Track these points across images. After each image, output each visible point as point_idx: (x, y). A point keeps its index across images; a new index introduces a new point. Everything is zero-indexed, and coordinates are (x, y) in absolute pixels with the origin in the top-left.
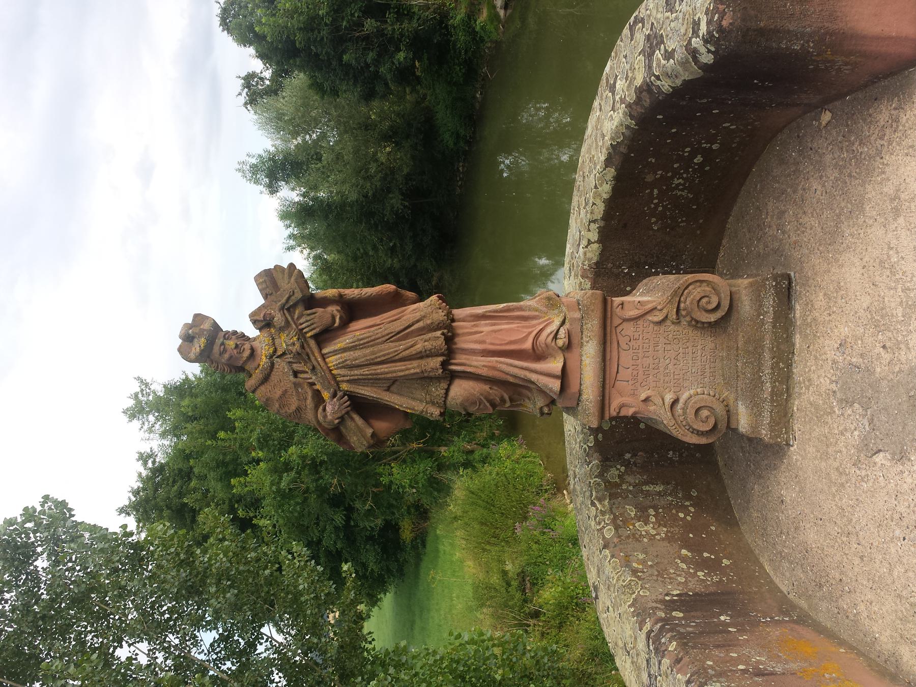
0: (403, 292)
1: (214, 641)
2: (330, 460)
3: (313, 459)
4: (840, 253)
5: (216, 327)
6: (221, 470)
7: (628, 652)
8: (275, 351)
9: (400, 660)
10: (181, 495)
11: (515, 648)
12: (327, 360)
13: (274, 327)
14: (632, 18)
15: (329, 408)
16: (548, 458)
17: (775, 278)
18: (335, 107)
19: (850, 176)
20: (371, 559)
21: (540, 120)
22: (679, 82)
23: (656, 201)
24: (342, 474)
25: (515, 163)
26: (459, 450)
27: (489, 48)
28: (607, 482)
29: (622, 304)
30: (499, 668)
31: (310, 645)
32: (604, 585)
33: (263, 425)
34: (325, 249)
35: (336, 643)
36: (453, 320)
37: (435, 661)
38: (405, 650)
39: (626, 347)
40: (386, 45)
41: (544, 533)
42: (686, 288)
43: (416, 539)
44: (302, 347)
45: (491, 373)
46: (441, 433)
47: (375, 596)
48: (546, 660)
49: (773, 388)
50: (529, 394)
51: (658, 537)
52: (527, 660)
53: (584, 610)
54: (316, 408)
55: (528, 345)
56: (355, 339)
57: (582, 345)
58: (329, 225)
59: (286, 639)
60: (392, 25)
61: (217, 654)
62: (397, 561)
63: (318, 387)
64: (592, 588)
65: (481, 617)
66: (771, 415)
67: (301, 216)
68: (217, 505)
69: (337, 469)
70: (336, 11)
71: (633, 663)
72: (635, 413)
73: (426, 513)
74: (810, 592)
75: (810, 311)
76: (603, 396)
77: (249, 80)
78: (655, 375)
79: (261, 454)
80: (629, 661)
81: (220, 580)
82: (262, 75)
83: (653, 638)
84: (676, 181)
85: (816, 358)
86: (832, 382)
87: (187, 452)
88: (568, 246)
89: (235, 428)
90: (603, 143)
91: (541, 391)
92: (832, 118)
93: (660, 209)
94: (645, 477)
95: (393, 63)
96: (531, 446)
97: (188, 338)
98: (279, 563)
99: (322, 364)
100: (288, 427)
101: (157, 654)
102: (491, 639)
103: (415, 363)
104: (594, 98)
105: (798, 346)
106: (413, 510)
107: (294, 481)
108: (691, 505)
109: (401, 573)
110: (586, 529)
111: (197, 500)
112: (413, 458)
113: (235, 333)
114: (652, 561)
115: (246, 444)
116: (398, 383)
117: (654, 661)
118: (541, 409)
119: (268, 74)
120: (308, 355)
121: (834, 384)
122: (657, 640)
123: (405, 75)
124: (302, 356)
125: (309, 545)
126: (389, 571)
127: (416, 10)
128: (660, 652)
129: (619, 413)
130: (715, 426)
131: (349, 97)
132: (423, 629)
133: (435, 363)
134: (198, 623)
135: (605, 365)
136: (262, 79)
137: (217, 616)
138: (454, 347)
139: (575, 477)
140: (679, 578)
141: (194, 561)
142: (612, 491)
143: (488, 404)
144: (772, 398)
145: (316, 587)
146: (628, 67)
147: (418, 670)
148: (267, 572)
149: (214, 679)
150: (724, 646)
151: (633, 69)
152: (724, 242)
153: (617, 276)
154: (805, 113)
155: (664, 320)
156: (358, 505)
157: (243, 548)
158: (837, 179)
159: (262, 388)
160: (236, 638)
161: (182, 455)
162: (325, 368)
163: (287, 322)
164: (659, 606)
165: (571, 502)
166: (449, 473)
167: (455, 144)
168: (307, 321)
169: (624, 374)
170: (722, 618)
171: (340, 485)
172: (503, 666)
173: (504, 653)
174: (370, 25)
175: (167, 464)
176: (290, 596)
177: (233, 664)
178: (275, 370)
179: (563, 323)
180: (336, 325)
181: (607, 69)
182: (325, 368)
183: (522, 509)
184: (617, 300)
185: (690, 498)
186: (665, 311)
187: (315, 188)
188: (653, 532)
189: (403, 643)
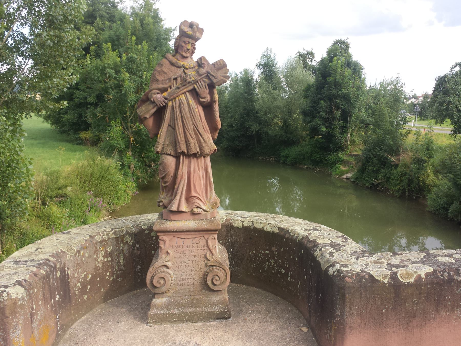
0: (218, 132)
1: (24, 35)
2: (123, 94)
3: (122, 86)
4: (242, 341)
5: (197, 40)
6: (115, 37)
7: (37, 250)
8: (187, 69)
9: (17, 133)
10: (101, 16)
11: (26, 193)
12: (183, 95)
13: (198, 69)
14: (347, 237)
15: (159, 96)
16: (128, 207)
17: (229, 311)
18: (299, 97)
19: (278, 342)
20: (69, 117)
21: (296, 197)
22: (319, 259)
23: (263, 252)
24: (115, 101)
25: (275, 185)
26: (130, 161)
27: (328, 171)
28: (124, 236)
29: (215, 239)
30: (14, 185)
31: (24, 85)
32: (71, 237)
33: (140, 60)
34: (230, 92)
35: (25, 98)
36: (204, 157)
37: (17, 152)
38: (22, 135)
39: (194, 242)
40: (328, 121)
41: (88, 206)
42: (223, 269)
43: (81, 140)
44: (189, 83)
45: (179, 176)
46: (139, 152)
47: (49, 119)
48: (20, 209)
49: (175, 314)
50: (169, 196)
51: (97, 263)
52: (20, 199)
53: (48, 228)
54: (159, 89)
55: (193, 194)
56: (194, 109)
57: (194, 220)
58: (242, 94)
59: (26, 72)
60: (338, 124)
61: (17, 36)
62: (69, 130)
63: (169, 90)
64: (68, 231)
65: (41, 175)
67: (247, 80)
68: (96, 35)
69: (117, 98)
70: (344, 97)
71: (32, 252)
72: (161, 248)
73: (95, 145)
74: (73, 339)
75: (214, 329)
76: (169, 232)
77: (311, 54)
78: (180, 257)
79: (124, 58)
80: (32, 251)
81: (57, 37)
82: (313, 61)
83: (46, 262)
84: (272, 261)
85: (191, 333)
86: (180, 342)
87: (124, 20)
88: (240, 212)
89: (137, 45)
91: (171, 201)
92: (305, 332)
93: (260, 255)
95: (320, 125)
96: (134, 198)
97: (191, 25)
98: (66, 68)
99: (181, 92)
100: (139, 72)
101: (16, 4)
102: (30, 180)
103: (183, 139)
104: (310, 221)
105: (196, 324)
106: (97, 138)
107: (111, 76)
108: (114, 278)
109: (63, 132)
110: (99, 227)
111: (98, 25)
112: (125, 137)
113: (195, 49)
114: (85, 260)
115: (129, 50)
116: (173, 130)
117: (34, 263)
118: (162, 201)
119: (314, 64)
120: (185, 85)
121: (179, 343)
122: (45, 264)
123: (314, 131)
124: (185, 82)
125: (77, 84)
126: (63, 126)
127: (345, 135)
128: (39, 266)
129: (161, 240)
130: (155, 287)
131: (304, 103)
132: (32, 145)
134: (33, 25)
135: (184, 232)
136: (311, 60)
137: (37, 36)
138: (192, 158)
139: (125, 220)
140: (76, 274)
141: (67, 23)
142: (119, 239)
143: (163, 175)
144: (171, 314)
145: (55, 87)
146: (325, 236)
147: (12, 142)
148: (62, 62)
149: (3, 34)
150: (44, 297)
151: (324, 238)
152: (244, 286)
153: (227, 236)
154: (306, 320)
155: (207, 259)
156: (99, 109)
157: (75, 49)
158: (276, 336)
159: (168, 62)
160: (26, 46)
161: (122, 18)
162: (179, 94)
163: (201, 75)
164: (62, 264)
165: (105, 220)
166: (118, 156)
167: (283, 156)
169: (180, 241)
170: (58, 296)
171: (109, 100)
172: (16, 187)
173: (23, 187)
174: (338, 113)
175: (117, 10)
176: (50, 74)
177: (12, 44)
178: (177, 69)
179: (205, 211)
180: (201, 100)
181: (323, 226)
182: (179, 94)
183: (100, 194)
184: (216, 236)
185: (117, 277)
186: (212, 259)
187: (260, 87)
188: (99, 260)
189: (26, 134)
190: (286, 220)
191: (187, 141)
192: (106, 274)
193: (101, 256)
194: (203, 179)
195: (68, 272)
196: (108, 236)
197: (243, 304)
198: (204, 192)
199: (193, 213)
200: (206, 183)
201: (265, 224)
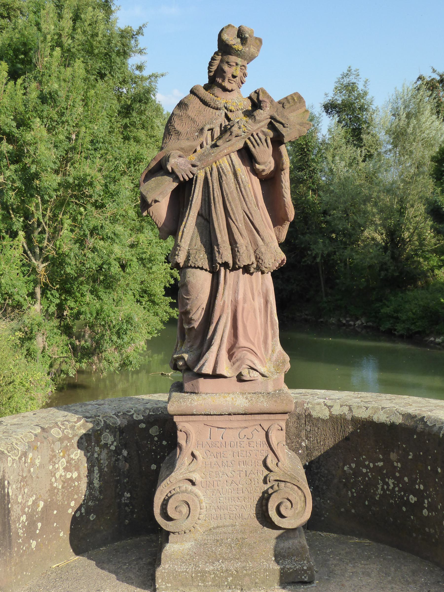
5: (251, 58)
23: (371, 465)
29: (282, 430)
39: (242, 436)
51: (53, 480)
56: (246, 184)
66: (183, 572)
84: (391, 482)
88: (323, 391)
90: (424, 411)
93: (364, 471)
94: (106, 469)
103: (226, 238)
108: (81, 514)
133: (227, 257)
140: (20, 497)
153: (298, 436)
168: (260, 139)
179: (263, 375)
180: (257, 166)
190: (417, 402)
191: (233, 243)
192: (69, 504)
193: (61, 468)
194: (260, 315)
195: (8, 489)
196: (74, 430)
197: (335, 562)
198: (262, 339)
199: (240, 378)
200: (266, 322)
201: (376, 410)
